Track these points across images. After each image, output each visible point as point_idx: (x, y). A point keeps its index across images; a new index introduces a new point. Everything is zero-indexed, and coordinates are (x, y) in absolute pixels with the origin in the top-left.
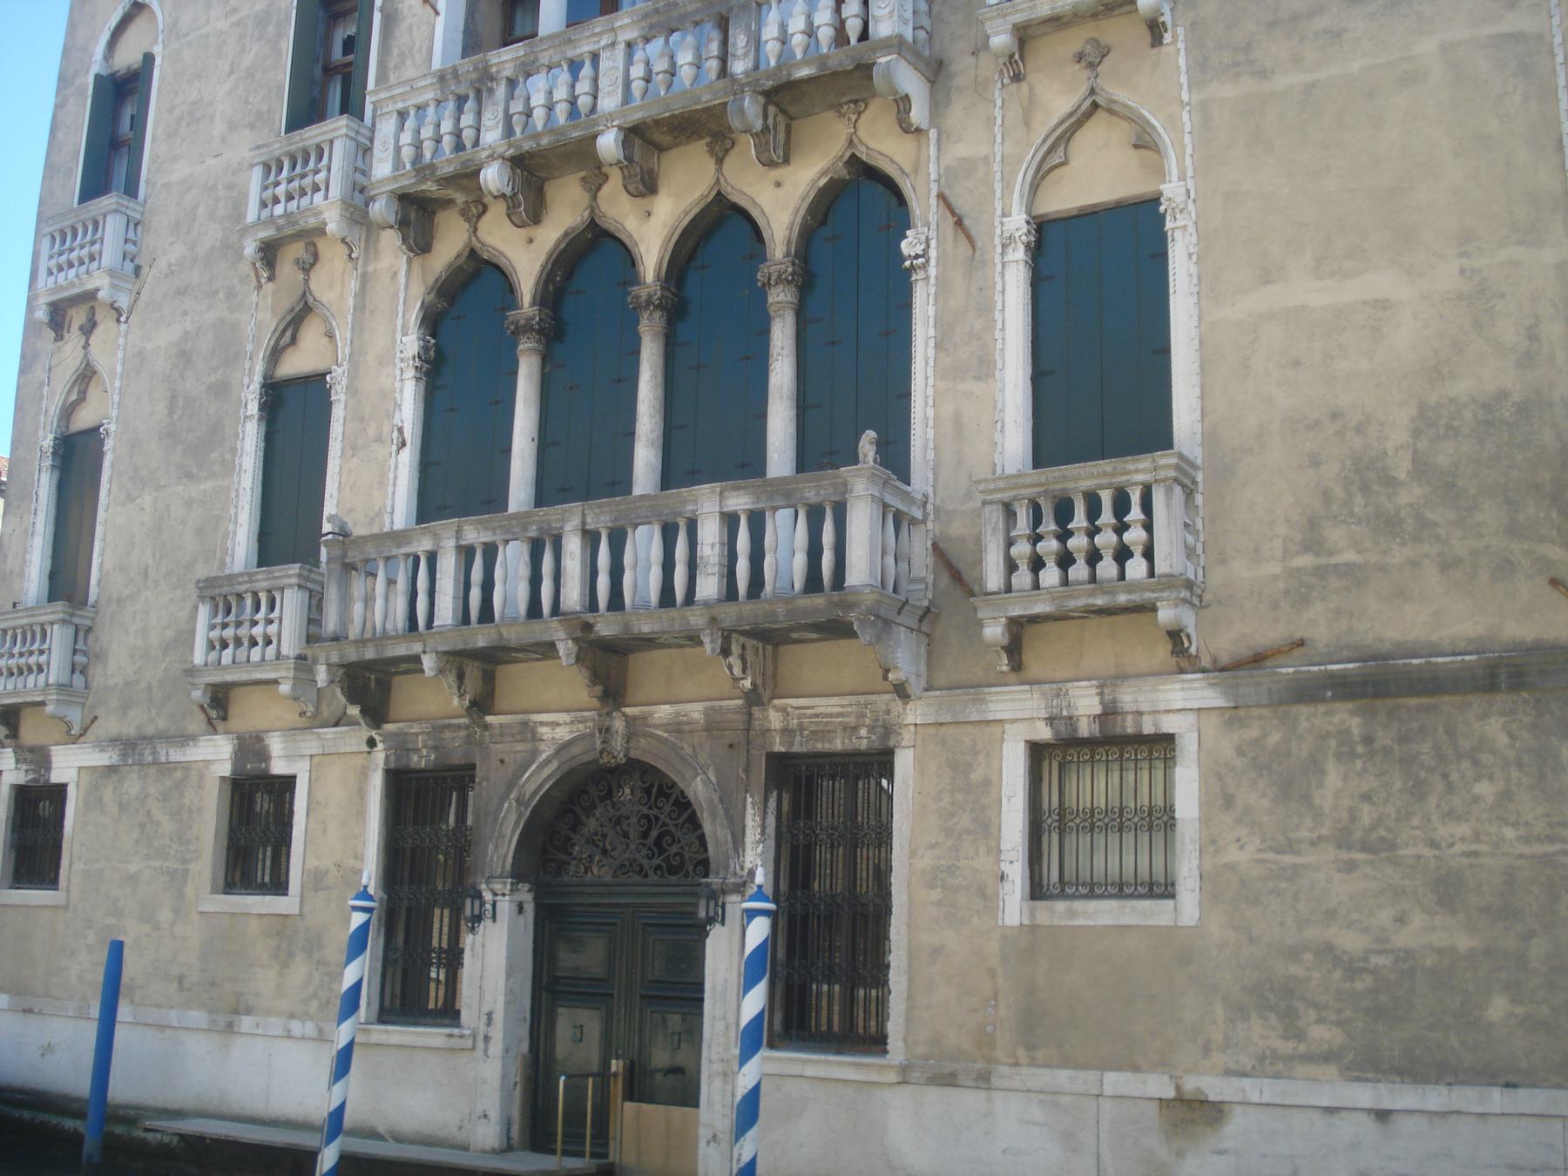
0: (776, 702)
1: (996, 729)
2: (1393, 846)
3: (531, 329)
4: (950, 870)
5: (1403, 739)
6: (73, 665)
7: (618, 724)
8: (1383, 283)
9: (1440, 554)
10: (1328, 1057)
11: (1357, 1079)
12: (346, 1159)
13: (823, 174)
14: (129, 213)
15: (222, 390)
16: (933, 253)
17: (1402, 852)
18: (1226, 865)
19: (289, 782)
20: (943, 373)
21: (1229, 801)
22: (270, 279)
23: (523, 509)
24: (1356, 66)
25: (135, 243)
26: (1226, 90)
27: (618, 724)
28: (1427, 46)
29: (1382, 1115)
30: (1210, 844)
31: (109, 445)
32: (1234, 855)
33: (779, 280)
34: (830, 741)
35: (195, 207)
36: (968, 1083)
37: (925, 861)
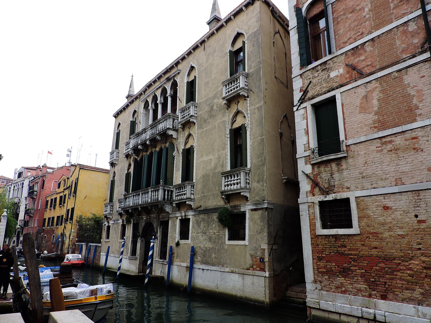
6: (191, 193)
8: (211, 157)
12: (120, 274)
16: (176, 155)
24: (210, 127)
26: (200, 131)
28: (216, 123)
29: (203, 269)
32: (194, 234)
37: (170, 235)
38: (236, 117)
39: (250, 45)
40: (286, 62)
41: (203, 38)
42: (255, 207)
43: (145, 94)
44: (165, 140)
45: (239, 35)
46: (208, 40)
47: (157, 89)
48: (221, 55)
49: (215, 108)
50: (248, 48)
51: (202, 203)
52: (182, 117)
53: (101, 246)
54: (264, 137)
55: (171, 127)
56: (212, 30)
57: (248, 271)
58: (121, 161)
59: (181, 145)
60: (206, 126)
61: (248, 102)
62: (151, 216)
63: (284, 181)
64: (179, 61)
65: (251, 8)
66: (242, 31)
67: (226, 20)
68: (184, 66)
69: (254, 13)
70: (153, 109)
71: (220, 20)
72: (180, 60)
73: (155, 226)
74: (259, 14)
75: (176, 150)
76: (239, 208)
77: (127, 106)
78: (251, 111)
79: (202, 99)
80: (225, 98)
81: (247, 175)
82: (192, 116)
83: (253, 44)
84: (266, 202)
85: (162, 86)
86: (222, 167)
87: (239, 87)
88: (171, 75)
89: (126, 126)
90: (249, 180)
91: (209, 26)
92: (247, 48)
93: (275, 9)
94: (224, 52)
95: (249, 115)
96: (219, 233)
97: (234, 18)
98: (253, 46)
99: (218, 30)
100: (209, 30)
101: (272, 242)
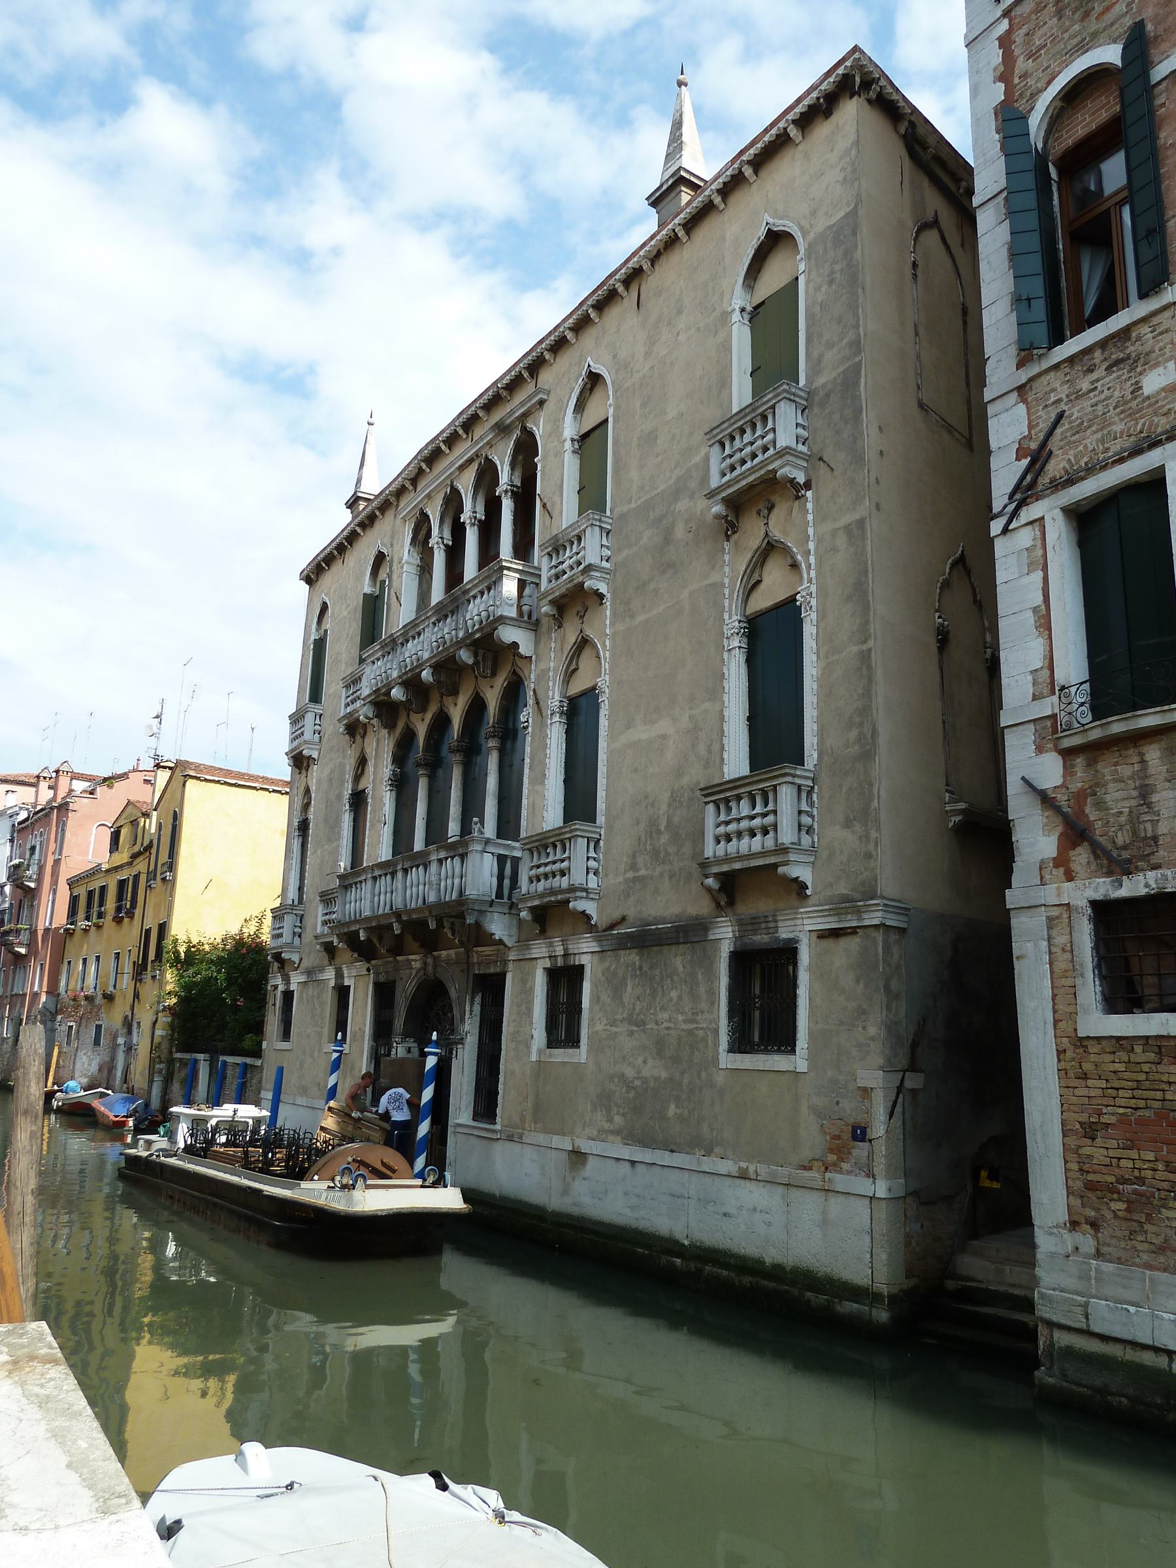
1: (535, 962)
4: (518, 1033)
5: (651, 968)
8: (664, 726)
13: (505, 680)
15: (339, 797)
16: (530, 720)
17: (647, 1027)
21: (598, 998)
22: (353, 743)
25: (320, 725)
26: (621, 627)
27: (430, 960)
28: (685, 594)
29: (633, 1163)
30: (592, 1020)
32: (599, 1027)
37: (511, 1029)
38: (762, 566)
41: (635, 259)
44: (489, 663)
46: (653, 265)
47: (462, 468)
48: (702, 325)
49: (679, 532)
51: (631, 910)
52: (553, 571)
54: (871, 643)
55: (513, 613)
56: (670, 227)
57: (807, 1174)
59: (551, 684)
60: (643, 607)
61: (809, 506)
62: (439, 957)
63: (958, 819)
64: (542, 353)
65: (822, 130)
69: (832, 150)
70: (446, 546)
73: (453, 993)
74: (853, 152)
76: (772, 925)
78: (820, 541)
79: (630, 502)
88: (512, 412)
90: (813, 817)
92: (807, 292)
93: (921, 130)
94: (714, 310)
96: (695, 1025)
97: (756, 172)
98: (831, 282)
99: (691, 224)
101: (904, 1062)
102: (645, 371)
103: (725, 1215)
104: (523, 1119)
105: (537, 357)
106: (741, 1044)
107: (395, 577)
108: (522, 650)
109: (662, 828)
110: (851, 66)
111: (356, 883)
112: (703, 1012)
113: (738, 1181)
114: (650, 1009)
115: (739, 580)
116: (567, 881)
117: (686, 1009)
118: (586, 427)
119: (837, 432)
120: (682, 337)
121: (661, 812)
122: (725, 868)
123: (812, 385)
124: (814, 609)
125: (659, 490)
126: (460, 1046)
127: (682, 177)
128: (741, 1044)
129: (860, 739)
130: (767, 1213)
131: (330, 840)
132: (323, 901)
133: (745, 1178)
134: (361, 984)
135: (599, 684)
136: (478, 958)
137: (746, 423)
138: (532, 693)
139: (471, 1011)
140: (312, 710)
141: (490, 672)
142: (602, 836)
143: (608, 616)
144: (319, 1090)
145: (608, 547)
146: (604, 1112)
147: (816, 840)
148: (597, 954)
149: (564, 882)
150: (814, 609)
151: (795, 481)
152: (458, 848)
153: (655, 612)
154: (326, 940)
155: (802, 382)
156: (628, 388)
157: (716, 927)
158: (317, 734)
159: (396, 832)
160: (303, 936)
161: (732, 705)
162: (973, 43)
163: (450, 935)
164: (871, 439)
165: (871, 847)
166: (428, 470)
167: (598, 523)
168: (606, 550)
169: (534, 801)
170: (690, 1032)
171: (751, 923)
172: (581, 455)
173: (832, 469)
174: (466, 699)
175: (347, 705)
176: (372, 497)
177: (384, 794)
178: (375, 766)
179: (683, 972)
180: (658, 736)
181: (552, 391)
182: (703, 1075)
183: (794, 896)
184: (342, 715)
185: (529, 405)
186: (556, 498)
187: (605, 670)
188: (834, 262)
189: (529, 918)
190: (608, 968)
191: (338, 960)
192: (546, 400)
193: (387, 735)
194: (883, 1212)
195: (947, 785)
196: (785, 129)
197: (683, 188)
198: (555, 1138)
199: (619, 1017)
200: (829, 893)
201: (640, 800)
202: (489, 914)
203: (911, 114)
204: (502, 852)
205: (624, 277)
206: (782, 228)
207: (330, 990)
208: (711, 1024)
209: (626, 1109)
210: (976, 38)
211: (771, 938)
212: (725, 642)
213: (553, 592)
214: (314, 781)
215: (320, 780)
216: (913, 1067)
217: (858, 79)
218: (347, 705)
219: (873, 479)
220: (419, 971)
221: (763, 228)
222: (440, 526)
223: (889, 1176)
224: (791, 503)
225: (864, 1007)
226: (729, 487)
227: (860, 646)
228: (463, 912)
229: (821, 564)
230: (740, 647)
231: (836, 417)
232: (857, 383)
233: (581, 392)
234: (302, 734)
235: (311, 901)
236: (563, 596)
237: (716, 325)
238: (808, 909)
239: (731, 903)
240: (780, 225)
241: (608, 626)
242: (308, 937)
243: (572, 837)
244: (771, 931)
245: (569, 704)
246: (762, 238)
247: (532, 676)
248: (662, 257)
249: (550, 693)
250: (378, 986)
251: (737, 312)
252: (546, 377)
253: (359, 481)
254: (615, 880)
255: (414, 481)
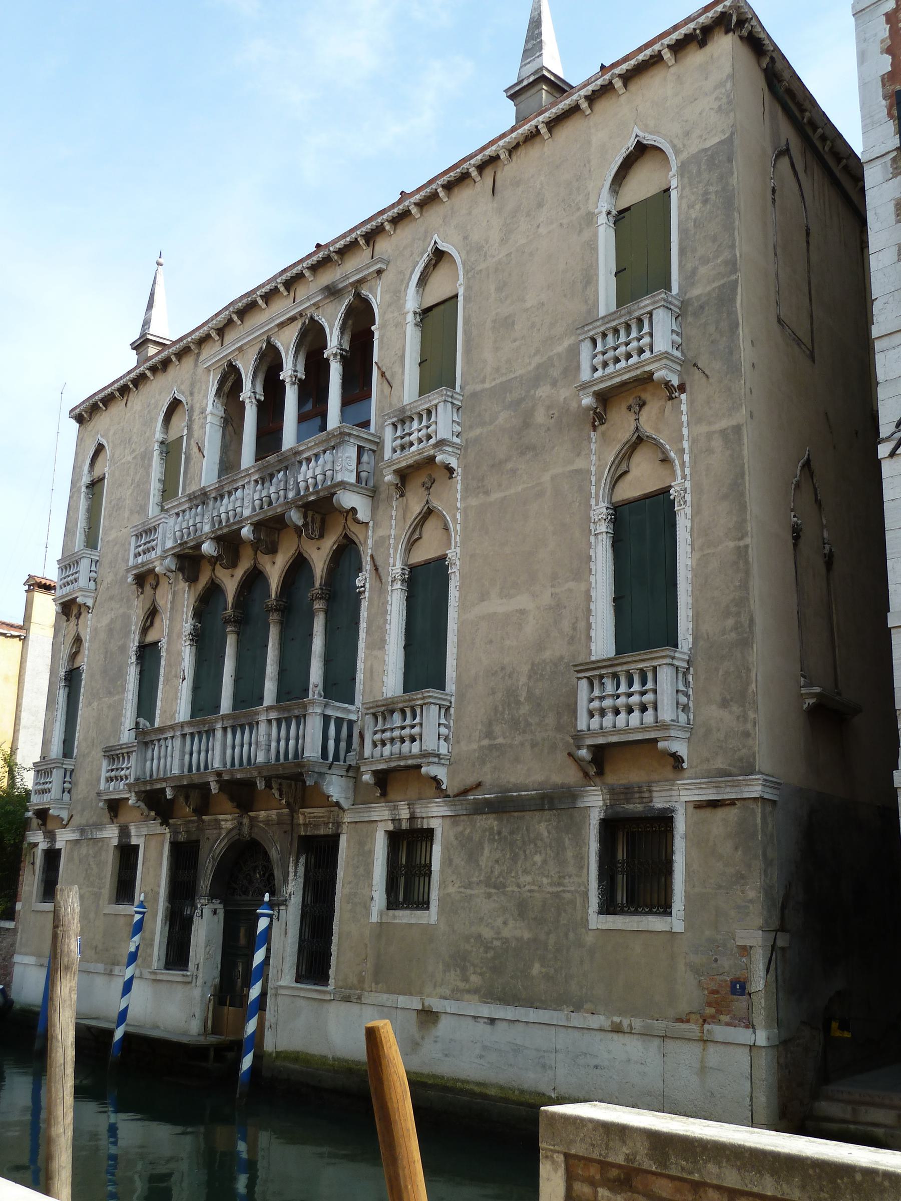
0: (301, 810)
1: (374, 825)
2: (505, 886)
3: (231, 621)
5: (512, 833)
6: (64, 789)
7: (246, 821)
8: (523, 601)
9: (531, 739)
10: (476, 991)
11: (485, 1002)
12: (126, 1035)
13: (335, 543)
14: (92, 557)
15: (123, 649)
16: (367, 585)
17: (507, 889)
18: (448, 894)
19: (138, 846)
20: (367, 648)
21: (451, 861)
22: (142, 593)
23: (228, 712)
24: (520, 488)
25: (96, 572)
26: (473, 502)
27: (246, 821)
28: (546, 478)
29: (492, 1021)
30: (443, 884)
31: (84, 676)
32: (451, 889)
33: (317, 598)
34: (319, 830)
35: (118, 554)
36: (354, 1001)
37: (347, 890)
38: (630, 458)
39: (693, 198)
40: (809, 261)
41: (494, 148)
42: (711, 795)
43: (226, 341)
44: (318, 525)
45: (641, 150)
46: (510, 155)
47: (281, 325)
48: (565, 221)
49: (540, 417)
50: (684, 206)
51: (487, 775)
52: (399, 442)
53: (14, 931)
54: (748, 540)
55: (352, 479)
56: (533, 123)
57: (683, 1026)
58: (111, 598)
59: (392, 551)
60: (500, 485)
61: (684, 407)
62: (256, 817)
63: (812, 701)
64: (382, 224)
65: (695, 58)
66: (655, 138)
67: (593, 91)
68: (405, 248)
69: (706, 79)
70: (258, 401)
71: (566, 88)
72: (386, 224)
73: (274, 854)
74: (729, 85)
75: (368, 567)
76: (646, 795)
77: (139, 380)
78: (694, 441)
79: (483, 381)
80: (591, 386)
81: (680, 675)
82: (441, 443)
83: (701, 192)
84: (758, 779)
85: (301, 315)
86: (569, 643)
87: (652, 351)
88: (346, 277)
89: (134, 458)
90: (688, 696)
91: (515, 105)
92: (679, 207)
93: (779, 65)
94: (579, 209)
95: (687, 458)
96: (561, 888)
97: (625, 85)
98: (705, 202)
99: (553, 124)
100: (513, 122)
101: (775, 923)
102: (500, 256)
103: (596, 1067)
104: (361, 980)
105: (377, 226)
106: (608, 907)
107: (196, 427)
108: (361, 516)
109: (522, 699)
110: (730, 6)
111: (159, 740)
112: (570, 876)
113: (611, 1035)
114: (511, 872)
115: (607, 470)
116: (418, 747)
117: (552, 873)
118: (429, 302)
119: (712, 342)
120: (542, 230)
121: (520, 683)
122: (601, 741)
123: (685, 295)
124: (689, 503)
125: (517, 374)
126: (282, 907)
127: (544, 76)
128: (608, 907)
129: (737, 627)
130: (642, 1064)
131: (110, 693)
132: (108, 756)
133: (618, 1032)
134: (153, 843)
135: (449, 556)
136: (304, 819)
137: (620, 324)
138: (369, 559)
139: (296, 873)
140: (88, 556)
141: (317, 534)
142: (453, 705)
143: (459, 490)
144: (96, 953)
145: (458, 424)
146: (458, 972)
147: (691, 718)
148: (449, 818)
149: (415, 748)
150: (689, 503)
151: (670, 383)
152: (293, 709)
153: (512, 491)
154: (113, 797)
155: (675, 289)
156: (481, 270)
157: (586, 796)
158: (92, 582)
159: (196, 688)
160: (72, 791)
161: (599, 585)
162: (861, 14)
163: (277, 796)
164: (746, 353)
165: (749, 726)
166: (239, 322)
167: (450, 400)
168: (457, 426)
169: (372, 666)
170: (557, 895)
171: (623, 793)
172: (422, 327)
173: (707, 376)
174: (287, 559)
175: (137, 555)
176: (168, 343)
177: (183, 648)
178: (171, 619)
179: (549, 837)
180: (517, 611)
181: (392, 263)
182: (571, 935)
183: (669, 768)
184: (131, 564)
185: (366, 272)
186: (397, 368)
187: (456, 543)
188: (709, 183)
189: (372, 782)
190: (462, 833)
191: (123, 819)
192: (384, 270)
193: (187, 589)
194: (764, 1061)
195: (802, 671)
196: (660, 51)
197: (544, 87)
198: (401, 998)
199: (475, 879)
200: (705, 767)
201: (496, 671)
202: (327, 776)
203: (773, 51)
204: (340, 715)
205: (480, 163)
206: (653, 143)
207: (111, 851)
208: (579, 887)
209: (484, 969)
210: (864, 10)
211: (645, 807)
212: (592, 527)
213: (399, 462)
214: (88, 630)
215: (96, 629)
216: (782, 928)
217: (734, 19)
218: (137, 555)
219: (748, 390)
220: (230, 831)
221: (632, 140)
222: (253, 381)
223: (768, 1027)
224: (664, 403)
225: (743, 872)
226: (602, 382)
227: (737, 542)
228: (301, 774)
229: (695, 463)
230: (607, 532)
231: (712, 329)
232: (733, 300)
233: (426, 267)
234: (76, 580)
235: (84, 756)
236: (409, 467)
237: (580, 225)
238: (686, 782)
239: (600, 773)
240: (649, 139)
241: (459, 500)
242: (82, 790)
243: (425, 704)
244: (645, 800)
245: (410, 572)
246: (631, 148)
247: (370, 542)
248: (520, 149)
249: (391, 560)
250: (175, 846)
251: (604, 215)
252: (383, 246)
253: (146, 323)
254: (469, 747)
255: (221, 332)
